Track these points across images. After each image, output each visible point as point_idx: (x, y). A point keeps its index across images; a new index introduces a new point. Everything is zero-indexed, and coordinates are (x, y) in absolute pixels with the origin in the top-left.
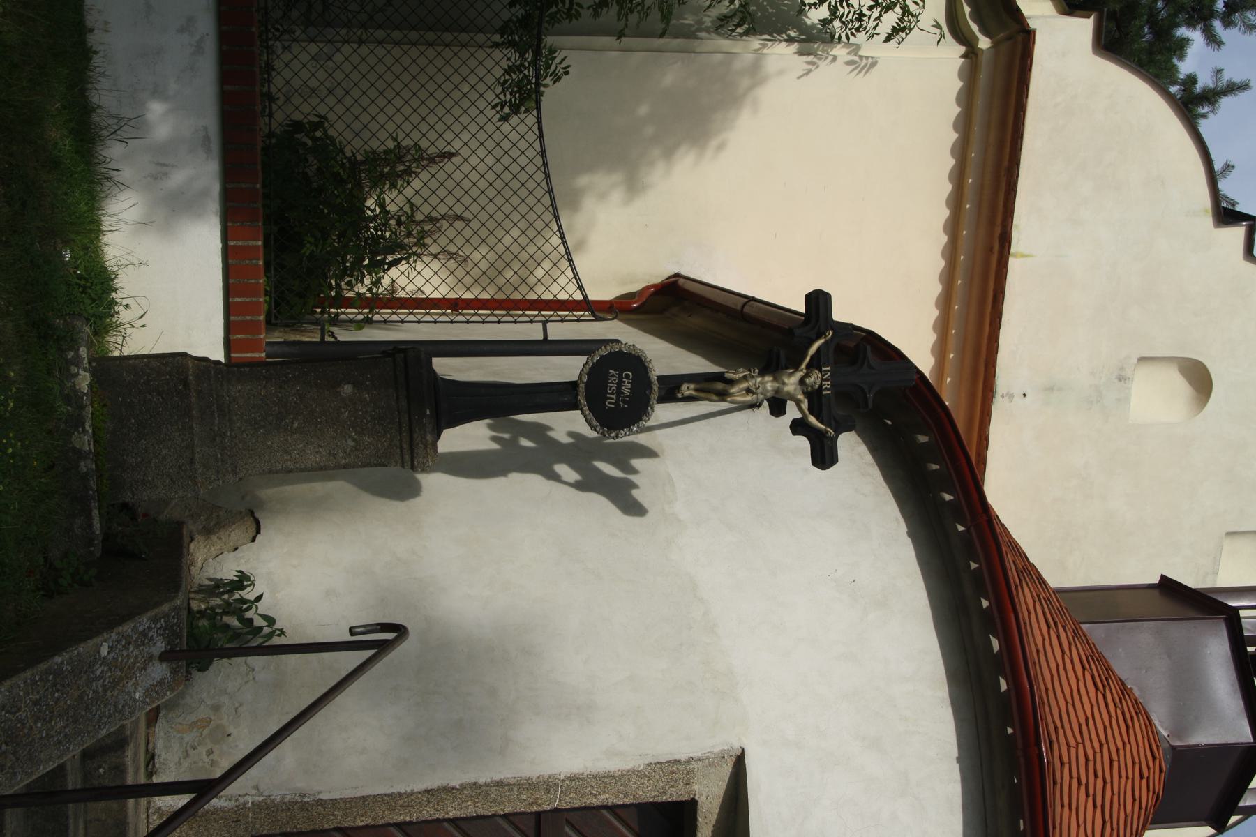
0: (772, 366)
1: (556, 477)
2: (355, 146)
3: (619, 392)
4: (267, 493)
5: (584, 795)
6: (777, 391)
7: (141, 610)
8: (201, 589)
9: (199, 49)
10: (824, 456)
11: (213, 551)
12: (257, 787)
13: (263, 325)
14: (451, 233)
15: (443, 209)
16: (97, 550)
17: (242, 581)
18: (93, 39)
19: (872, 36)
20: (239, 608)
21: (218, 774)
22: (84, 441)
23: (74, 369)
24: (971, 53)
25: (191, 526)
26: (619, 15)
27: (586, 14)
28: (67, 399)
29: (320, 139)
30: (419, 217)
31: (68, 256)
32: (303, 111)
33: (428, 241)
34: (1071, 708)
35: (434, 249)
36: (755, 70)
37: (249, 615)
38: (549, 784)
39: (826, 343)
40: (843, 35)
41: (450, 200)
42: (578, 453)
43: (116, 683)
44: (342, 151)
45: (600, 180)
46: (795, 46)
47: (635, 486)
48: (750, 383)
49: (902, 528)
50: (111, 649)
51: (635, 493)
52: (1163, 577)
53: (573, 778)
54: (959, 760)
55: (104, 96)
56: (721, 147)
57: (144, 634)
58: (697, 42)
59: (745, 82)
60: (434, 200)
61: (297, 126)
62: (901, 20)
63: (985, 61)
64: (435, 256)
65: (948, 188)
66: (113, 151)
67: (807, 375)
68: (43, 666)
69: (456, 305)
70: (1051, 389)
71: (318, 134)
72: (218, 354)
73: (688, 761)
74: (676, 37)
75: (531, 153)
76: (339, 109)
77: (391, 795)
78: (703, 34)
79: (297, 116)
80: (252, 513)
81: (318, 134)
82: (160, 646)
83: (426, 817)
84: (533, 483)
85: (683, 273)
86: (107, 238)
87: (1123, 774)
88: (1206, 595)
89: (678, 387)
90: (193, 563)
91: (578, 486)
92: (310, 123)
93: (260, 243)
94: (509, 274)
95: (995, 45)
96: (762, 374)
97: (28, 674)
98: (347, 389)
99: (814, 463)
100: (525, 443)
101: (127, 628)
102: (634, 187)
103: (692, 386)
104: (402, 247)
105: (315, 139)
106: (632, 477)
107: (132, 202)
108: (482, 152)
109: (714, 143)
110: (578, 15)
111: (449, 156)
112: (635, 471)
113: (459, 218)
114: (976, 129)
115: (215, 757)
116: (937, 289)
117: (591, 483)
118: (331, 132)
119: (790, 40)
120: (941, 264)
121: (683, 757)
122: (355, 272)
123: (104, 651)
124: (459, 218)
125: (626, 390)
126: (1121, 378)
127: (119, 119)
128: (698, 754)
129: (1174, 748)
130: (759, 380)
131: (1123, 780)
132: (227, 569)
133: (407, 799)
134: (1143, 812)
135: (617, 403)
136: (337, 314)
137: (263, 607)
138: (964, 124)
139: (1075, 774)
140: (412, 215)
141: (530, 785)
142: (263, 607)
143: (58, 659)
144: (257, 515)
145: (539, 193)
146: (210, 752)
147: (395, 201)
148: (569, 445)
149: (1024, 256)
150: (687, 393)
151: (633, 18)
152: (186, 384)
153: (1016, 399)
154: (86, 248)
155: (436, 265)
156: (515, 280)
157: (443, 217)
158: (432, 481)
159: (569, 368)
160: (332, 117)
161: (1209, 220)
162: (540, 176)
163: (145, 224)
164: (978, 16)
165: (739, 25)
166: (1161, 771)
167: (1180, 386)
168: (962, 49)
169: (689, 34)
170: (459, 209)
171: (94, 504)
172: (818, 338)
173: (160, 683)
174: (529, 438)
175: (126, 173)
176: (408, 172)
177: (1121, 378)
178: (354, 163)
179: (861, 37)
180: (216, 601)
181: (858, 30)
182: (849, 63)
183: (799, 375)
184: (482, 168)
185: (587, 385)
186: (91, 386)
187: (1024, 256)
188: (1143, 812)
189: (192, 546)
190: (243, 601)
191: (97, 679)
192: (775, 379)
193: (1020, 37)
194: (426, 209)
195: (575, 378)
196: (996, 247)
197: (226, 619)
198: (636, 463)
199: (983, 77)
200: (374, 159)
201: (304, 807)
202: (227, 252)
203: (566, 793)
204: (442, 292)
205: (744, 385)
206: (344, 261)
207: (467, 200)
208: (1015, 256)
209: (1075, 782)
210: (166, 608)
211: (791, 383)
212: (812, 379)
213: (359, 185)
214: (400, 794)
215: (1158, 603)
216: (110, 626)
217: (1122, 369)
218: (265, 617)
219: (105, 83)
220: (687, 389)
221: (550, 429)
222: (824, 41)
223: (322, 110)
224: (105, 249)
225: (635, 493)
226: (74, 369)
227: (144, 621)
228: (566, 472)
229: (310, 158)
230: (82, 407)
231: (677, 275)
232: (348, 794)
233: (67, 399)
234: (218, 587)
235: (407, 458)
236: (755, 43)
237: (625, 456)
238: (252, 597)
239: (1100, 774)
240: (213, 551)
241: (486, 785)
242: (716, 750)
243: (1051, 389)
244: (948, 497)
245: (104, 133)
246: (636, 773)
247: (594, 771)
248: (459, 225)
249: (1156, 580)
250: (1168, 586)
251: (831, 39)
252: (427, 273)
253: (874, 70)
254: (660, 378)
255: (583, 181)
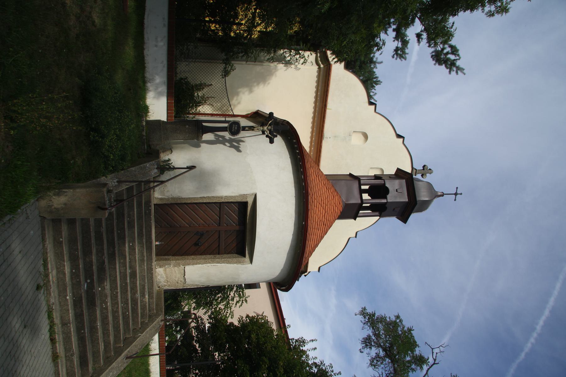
0: (263, 125)
1: (226, 145)
2: (193, 82)
3: (235, 129)
4: (174, 146)
5: (228, 200)
6: (263, 129)
7: (154, 160)
8: (162, 161)
9: (164, 67)
10: (272, 142)
11: (164, 155)
12: (171, 195)
13: (174, 116)
14: (211, 100)
15: (210, 96)
16: (146, 151)
17: (169, 160)
18: (146, 65)
19: (299, 64)
20: (169, 165)
21: (166, 180)
22: (144, 133)
23: (143, 121)
24: (319, 68)
25: (160, 151)
26: (246, 58)
27: (240, 58)
28: (142, 126)
29: (186, 82)
30: (205, 97)
31: (142, 103)
32: (183, 76)
33: (207, 102)
34: (319, 191)
35: (208, 103)
36: (276, 69)
37: (170, 166)
38: (222, 197)
39: (272, 122)
40: (293, 63)
41: (211, 94)
42: (230, 141)
43: (149, 171)
44: (190, 84)
45: (245, 89)
46: (284, 65)
47: (240, 147)
48: (258, 128)
49: (289, 156)
50: (149, 166)
51: (240, 148)
52: (350, 173)
53: (226, 197)
54: (295, 197)
55: (147, 75)
56: (268, 84)
57: (154, 164)
58: (263, 63)
59: (274, 71)
60: (208, 94)
61: (182, 79)
62: (304, 60)
63: (322, 69)
64: (208, 105)
65: (314, 95)
66: (149, 85)
67: (268, 127)
68: (139, 166)
69: (212, 115)
70: (335, 137)
71: (186, 80)
72: (165, 120)
73: (246, 195)
74: (259, 62)
75: (223, 86)
76: (190, 76)
77: (194, 198)
78: (265, 62)
79: (182, 77)
80: (171, 149)
81: (186, 80)
82: (156, 167)
83: (200, 202)
84: (221, 146)
85: (259, 110)
86: (147, 100)
87: (331, 204)
88: (358, 178)
89: (245, 128)
90: (161, 157)
91: (230, 147)
92: (185, 78)
93: (173, 101)
94: (225, 108)
95: (324, 66)
96: (260, 126)
97: (137, 167)
98: (187, 126)
99: (270, 143)
100: (220, 139)
101: (151, 162)
102: (251, 91)
103: (248, 128)
104: (201, 103)
105: (185, 81)
106: (240, 146)
107: (152, 94)
108: (219, 84)
109: (267, 83)
110: (238, 58)
111: (211, 85)
112: (240, 145)
113: (213, 97)
114: (320, 83)
115: (165, 189)
116: (312, 115)
117: (232, 146)
118: (189, 80)
119: (283, 63)
120: (313, 110)
121: (246, 194)
122: (192, 107)
123: (148, 165)
124: (213, 97)
125: (236, 128)
126: (350, 135)
127: (150, 79)
128: (248, 193)
129: (346, 203)
130: (260, 127)
131: (331, 206)
132: (167, 158)
133: (197, 198)
134: (336, 213)
135: (234, 130)
136: (188, 116)
137: (173, 164)
138: (318, 82)
139: (318, 201)
140: (204, 97)
141: (219, 197)
142: (173, 164)
143: (141, 165)
144: (172, 149)
145: (225, 93)
146: (164, 189)
147: (200, 94)
148: (228, 140)
149: (330, 109)
150: (247, 129)
151: (249, 59)
152: (160, 124)
153: (328, 138)
154: (144, 102)
155: (208, 106)
156: (226, 109)
157: (210, 97)
158: (203, 145)
159: (226, 125)
160: (188, 77)
161: (367, 104)
162: (225, 90)
163: (154, 98)
164: (321, 60)
165: (271, 60)
166: (341, 206)
167: (362, 138)
168: (318, 67)
169: (262, 62)
170: (213, 96)
171: (145, 144)
172: (271, 120)
173: (156, 172)
174: (221, 138)
175: (151, 88)
176: (203, 88)
177: (350, 135)
178: (193, 86)
179: (297, 64)
180: (165, 164)
181: (296, 62)
182: (295, 68)
183: (267, 127)
184: (219, 87)
185: (229, 127)
186: (145, 124)
187: (330, 109)
188: (336, 213)
189: (161, 154)
190: (169, 164)
191: (147, 170)
192: (263, 127)
193: (329, 65)
194: (207, 96)
195: (227, 126)
196: (324, 107)
197: (166, 167)
198: (241, 143)
199: (321, 73)
200: (196, 85)
201: (179, 199)
202: (168, 103)
203: (225, 199)
204: (211, 112)
205: (257, 128)
206: (190, 105)
207: (214, 94)
208: (328, 109)
209: (318, 203)
210: (157, 160)
211: (265, 128)
212: (269, 128)
213: (193, 90)
214: (196, 198)
215: (349, 178)
216: (148, 162)
217: (350, 133)
218: (173, 166)
219: (147, 73)
220: (247, 129)
221: (225, 137)
222: (289, 64)
223: (187, 76)
224: (147, 102)
225: (240, 148)
226: (143, 121)
227: (154, 162)
228: (227, 144)
229: (184, 85)
230: (144, 128)
231: (258, 110)
232: (187, 197)
233: (142, 126)
234: (165, 161)
235: (197, 138)
236: (276, 63)
237: (239, 141)
238: (171, 163)
239: (325, 203)
240: (164, 155)
241: (211, 197)
242: (251, 193)
243: (335, 137)
244: (298, 151)
245: (147, 81)
246: (237, 196)
247: (230, 195)
248: (213, 99)
249: (349, 174)
250: (351, 175)
251: (291, 64)
252: (207, 107)
253: (300, 70)
254: (242, 127)
255: (240, 90)
